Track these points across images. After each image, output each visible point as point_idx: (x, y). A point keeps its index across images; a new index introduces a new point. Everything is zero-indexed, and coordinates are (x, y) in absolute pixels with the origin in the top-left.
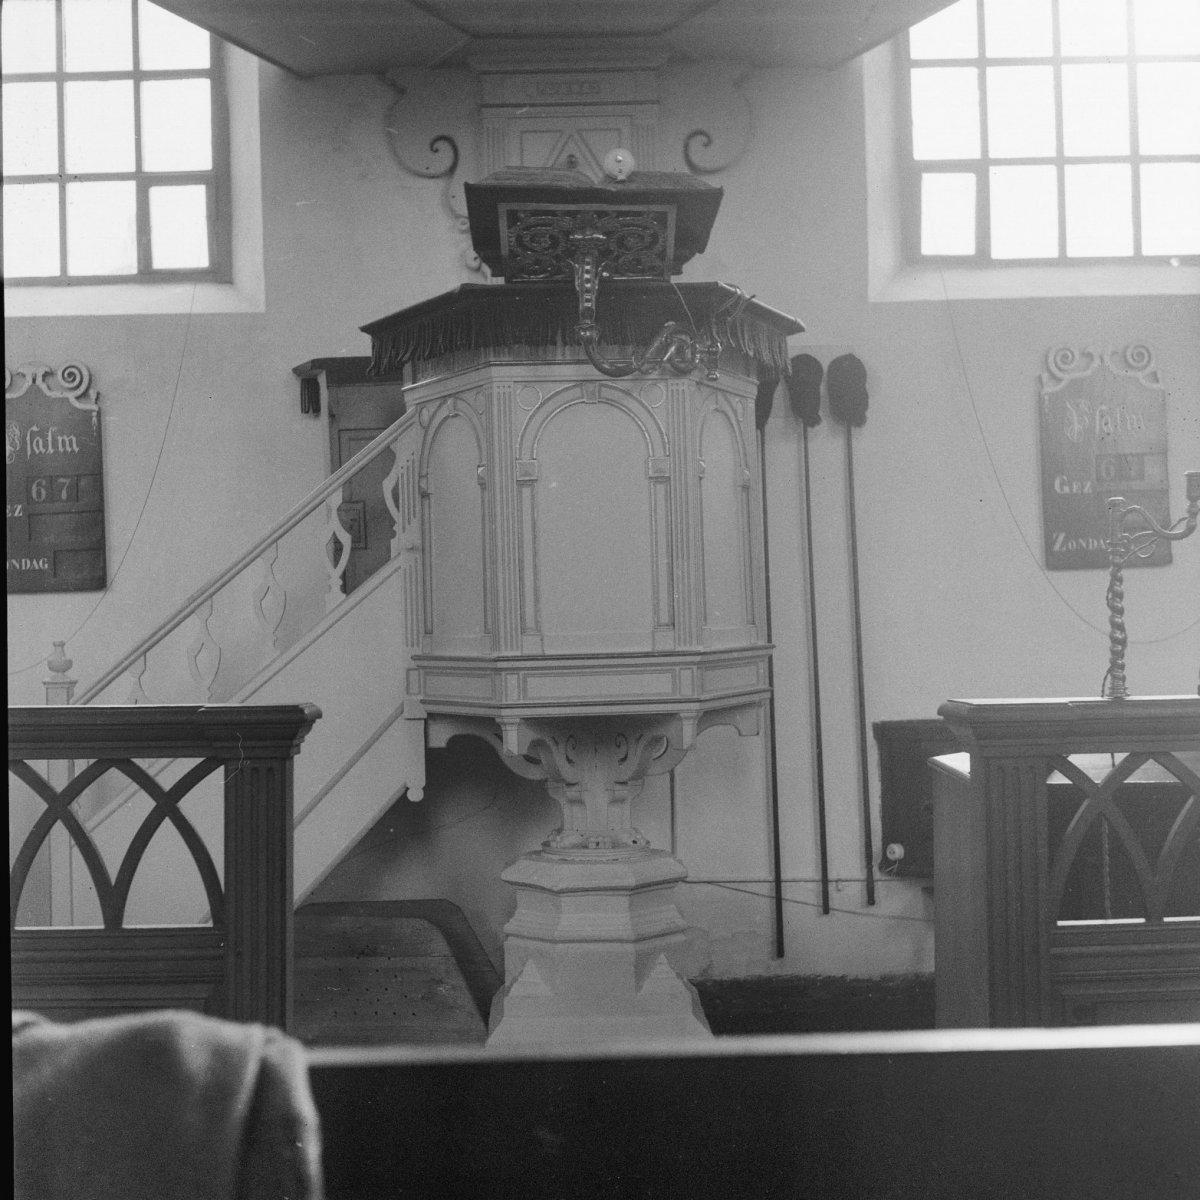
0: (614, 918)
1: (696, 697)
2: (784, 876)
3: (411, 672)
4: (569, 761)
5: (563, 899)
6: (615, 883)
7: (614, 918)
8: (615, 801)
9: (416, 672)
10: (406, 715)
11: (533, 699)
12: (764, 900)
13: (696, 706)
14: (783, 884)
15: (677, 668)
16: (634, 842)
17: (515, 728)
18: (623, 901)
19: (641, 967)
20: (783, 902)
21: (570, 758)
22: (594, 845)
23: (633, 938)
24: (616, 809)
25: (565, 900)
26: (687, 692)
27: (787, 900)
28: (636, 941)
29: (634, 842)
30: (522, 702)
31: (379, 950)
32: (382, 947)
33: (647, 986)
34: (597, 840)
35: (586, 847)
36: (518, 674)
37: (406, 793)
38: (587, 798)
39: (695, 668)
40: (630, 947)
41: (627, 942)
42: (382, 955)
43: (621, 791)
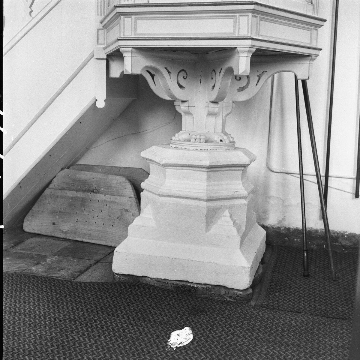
0: (197, 185)
1: (249, 35)
2: (330, 174)
3: (100, 31)
4: (181, 86)
5: (167, 170)
6: (200, 163)
7: (197, 185)
8: (210, 114)
9: (103, 31)
10: (95, 57)
11: (140, 34)
12: (349, 194)
13: (249, 42)
14: (329, 178)
15: (237, 15)
16: (221, 141)
17: (130, 54)
18: (203, 175)
19: (211, 216)
20: (329, 188)
21: (182, 84)
22: (194, 140)
23: (205, 198)
24: (212, 119)
25: (169, 170)
26: (244, 33)
27: (331, 187)
28: (207, 200)
29: (221, 141)
30: (133, 36)
31: (100, 191)
32: (102, 189)
33: (214, 229)
34: (195, 137)
35: (190, 141)
36: (131, 17)
37: (95, 103)
38: (193, 110)
39: (250, 15)
40: (204, 204)
41: (203, 200)
42: (102, 193)
43: (216, 108)
